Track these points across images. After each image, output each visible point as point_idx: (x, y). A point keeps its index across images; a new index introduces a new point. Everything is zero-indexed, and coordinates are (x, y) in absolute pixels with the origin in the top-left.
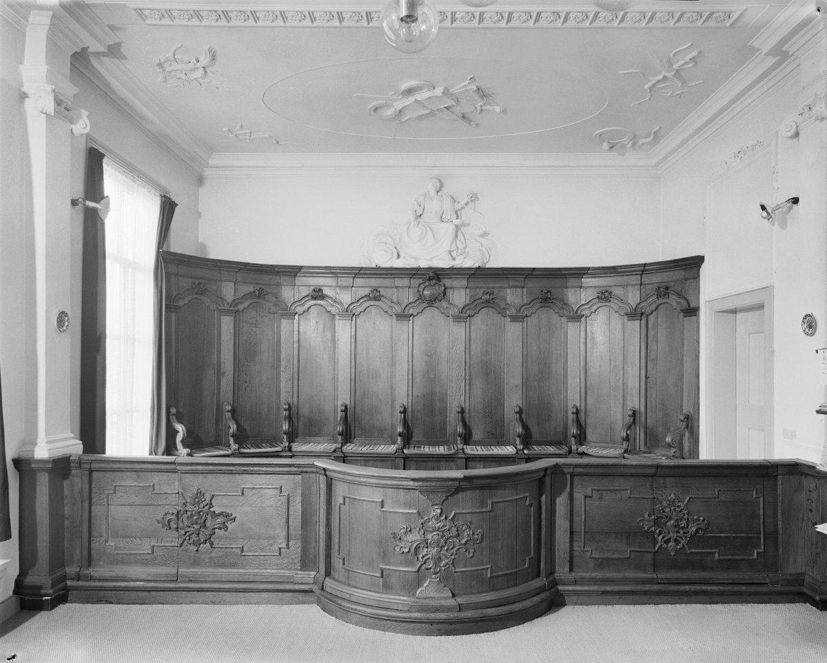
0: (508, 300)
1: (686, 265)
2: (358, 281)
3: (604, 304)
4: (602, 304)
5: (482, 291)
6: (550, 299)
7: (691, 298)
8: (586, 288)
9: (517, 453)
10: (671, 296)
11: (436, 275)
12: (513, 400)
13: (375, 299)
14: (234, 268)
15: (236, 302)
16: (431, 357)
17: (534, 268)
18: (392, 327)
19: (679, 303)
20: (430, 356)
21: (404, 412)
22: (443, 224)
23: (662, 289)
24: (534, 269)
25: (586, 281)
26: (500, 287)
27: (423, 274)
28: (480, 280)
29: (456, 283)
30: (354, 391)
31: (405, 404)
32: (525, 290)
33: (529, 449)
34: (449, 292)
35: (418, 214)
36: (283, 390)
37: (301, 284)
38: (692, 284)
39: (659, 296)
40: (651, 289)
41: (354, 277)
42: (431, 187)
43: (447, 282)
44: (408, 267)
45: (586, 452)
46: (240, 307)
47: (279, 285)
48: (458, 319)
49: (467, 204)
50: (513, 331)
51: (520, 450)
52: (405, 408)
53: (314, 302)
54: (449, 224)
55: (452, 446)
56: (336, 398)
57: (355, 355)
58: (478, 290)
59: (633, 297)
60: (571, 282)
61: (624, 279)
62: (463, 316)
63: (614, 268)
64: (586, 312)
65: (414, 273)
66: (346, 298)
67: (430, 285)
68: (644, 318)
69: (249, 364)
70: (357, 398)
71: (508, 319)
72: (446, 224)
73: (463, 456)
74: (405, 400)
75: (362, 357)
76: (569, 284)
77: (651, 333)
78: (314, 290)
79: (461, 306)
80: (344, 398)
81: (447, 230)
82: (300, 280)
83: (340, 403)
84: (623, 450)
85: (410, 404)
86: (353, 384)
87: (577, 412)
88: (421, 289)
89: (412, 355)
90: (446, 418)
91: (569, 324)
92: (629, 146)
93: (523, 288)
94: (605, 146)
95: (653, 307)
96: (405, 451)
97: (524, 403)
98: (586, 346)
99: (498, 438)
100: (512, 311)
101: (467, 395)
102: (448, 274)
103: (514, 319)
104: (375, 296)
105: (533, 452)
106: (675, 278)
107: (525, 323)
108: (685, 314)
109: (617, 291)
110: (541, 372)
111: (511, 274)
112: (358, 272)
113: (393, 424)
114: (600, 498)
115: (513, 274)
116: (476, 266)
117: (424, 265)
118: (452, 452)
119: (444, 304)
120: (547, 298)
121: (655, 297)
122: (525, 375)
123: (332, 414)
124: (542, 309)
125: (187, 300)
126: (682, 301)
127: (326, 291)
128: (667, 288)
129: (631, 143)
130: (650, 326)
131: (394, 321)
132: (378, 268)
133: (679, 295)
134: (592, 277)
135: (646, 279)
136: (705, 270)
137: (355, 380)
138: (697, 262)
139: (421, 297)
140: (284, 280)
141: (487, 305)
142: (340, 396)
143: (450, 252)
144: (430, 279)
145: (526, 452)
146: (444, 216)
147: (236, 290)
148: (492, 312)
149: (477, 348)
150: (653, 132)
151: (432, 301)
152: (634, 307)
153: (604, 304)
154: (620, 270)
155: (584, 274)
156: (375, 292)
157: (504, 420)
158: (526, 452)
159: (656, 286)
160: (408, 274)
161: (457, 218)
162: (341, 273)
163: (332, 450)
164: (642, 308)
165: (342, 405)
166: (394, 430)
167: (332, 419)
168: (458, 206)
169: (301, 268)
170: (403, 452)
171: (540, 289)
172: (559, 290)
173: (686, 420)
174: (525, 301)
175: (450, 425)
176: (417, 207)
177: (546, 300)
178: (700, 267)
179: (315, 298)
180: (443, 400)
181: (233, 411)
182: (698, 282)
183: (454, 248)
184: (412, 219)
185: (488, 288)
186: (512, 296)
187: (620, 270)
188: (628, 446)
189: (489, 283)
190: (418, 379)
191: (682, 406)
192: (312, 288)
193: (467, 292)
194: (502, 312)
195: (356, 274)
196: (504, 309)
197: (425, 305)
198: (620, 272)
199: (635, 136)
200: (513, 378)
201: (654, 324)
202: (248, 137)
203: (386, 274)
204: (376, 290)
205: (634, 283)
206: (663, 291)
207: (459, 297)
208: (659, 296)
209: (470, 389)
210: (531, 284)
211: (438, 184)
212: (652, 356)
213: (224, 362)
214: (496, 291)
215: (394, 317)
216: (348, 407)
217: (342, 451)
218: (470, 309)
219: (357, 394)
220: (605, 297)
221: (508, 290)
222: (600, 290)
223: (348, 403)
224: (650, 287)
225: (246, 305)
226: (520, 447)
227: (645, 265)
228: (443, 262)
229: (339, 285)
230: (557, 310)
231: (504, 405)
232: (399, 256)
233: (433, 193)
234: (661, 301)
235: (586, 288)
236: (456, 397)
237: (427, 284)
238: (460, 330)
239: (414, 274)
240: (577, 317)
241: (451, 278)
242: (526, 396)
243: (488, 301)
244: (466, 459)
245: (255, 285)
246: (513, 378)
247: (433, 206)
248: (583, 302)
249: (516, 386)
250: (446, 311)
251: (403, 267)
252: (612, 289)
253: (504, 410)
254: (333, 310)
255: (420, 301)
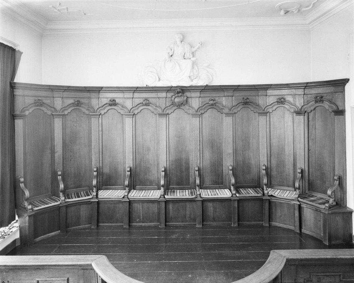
0: (224, 103)
1: (335, 84)
2: (136, 95)
3: (280, 105)
4: (279, 106)
5: (208, 99)
6: (248, 102)
7: (339, 103)
8: (270, 96)
9: (232, 196)
10: (324, 102)
11: (182, 90)
12: (228, 163)
13: (147, 105)
14: (62, 89)
15: (64, 109)
16: (180, 139)
17: (239, 85)
18: (156, 121)
19: (329, 106)
20: (179, 137)
21: (165, 171)
22: (185, 60)
23: (318, 98)
24: (239, 86)
25: (269, 92)
26: (219, 96)
27: (174, 90)
28: (208, 92)
29: (193, 94)
30: (135, 159)
31: (165, 166)
32: (234, 97)
33: (239, 193)
34: (190, 100)
35: (171, 55)
36: (93, 159)
37: (102, 97)
38: (340, 95)
39: (316, 102)
40: (311, 97)
41: (304, 88)
42: (178, 39)
43: (188, 94)
44: (165, 86)
45: (273, 195)
46: (66, 112)
47: (90, 98)
48: (194, 115)
49: (198, 48)
50: (228, 121)
51: (234, 194)
52: (165, 168)
53: (110, 107)
54: (188, 60)
55: (193, 190)
56: (125, 163)
57: (135, 137)
58: (206, 99)
59: (299, 102)
60: (261, 93)
61: (294, 91)
62: (199, 113)
63: (287, 84)
64: (271, 110)
65: (169, 89)
66: (129, 104)
67: (178, 96)
68: (306, 114)
69: (72, 145)
70: (137, 163)
71: (224, 115)
72: (187, 60)
73: (200, 199)
74: (165, 163)
75: (140, 139)
76: (259, 94)
77: (311, 123)
78: (110, 100)
79: (196, 108)
80: (129, 163)
81: (187, 64)
82: (102, 95)
83: (127, 166)
84: (297, 196)
85: (168, 168)
86: (134, 155)
87: (266, 169)
88: (173, 99)
89: (169, 137)
90: (189, 173)
91: (260, 117)
92: (295, 12)
93: (232, 96)
94: (282, 12)
95: (312, 108)
96: (166, 197)
97: (234, 163)
98: (270, 130)
99: (219, 183)
100: (226, 111)
101: (201, 160)
102: (189, 90)
103: (228, 115)
104: (147, 103)
105: (242, 195)
106: (327, 91)
107: (234, 117)
108: (336, 114)
109: (289, 98)
110: (243, 144)
111: (225, 89)
112: (136, 90)
113: (158, 178)
114: (318, 281)
115: (227, 89)
116: (205, 84)
117: (174, 84)
118: (194, 196)
119: (187, 107)
120: (247, 102)
121: (314, 102)
122: (234, 148)
123: (123, 172)
124: (244, 109)
125: (31, 111)
126: (333, 105)
127: (118, 101)
128: (322, 97)
129: (297, 11)
130: (310, 120)
131: (158, 117)
132: (147, 87)
133: (330, 102)
134: (273, 90)
135: (307, 91)
136: (348, 87)
137: (135, 152)
138: (345, 82)
139: (173, 104)
140: (93, 95)
141: (212, 107)
142: (127, 162)
143: (190, 77)
144: (178, 93)
145: (237, 195)
146: (185, 56)
147: (63, 102)
148: (214, 111)
149: (206, 132)
150: (313, 3)
151: (180, 105)
152: (300, 108)
153: (280, 105)
154: (291, 86)
155: (268, 88)
156: (146, 101)
157: (223, 174)
158: (237, 195)
159: (314, 96)
160: (132, 90)
161: (193, 56)
162: (126, 90)
163: (122, 196)
164: (305, 109)
165: (128, 167)
166: (159, 182)
167: (123, 174)
168: (193, 50)
169: (102, 88)
170: (164, 197)
171: (243, 97)
172: (254, 97)
173: (338, 180)
174: (234, 105)
175: (192, 177)
176: (169, 51)
177: (246, 103)
178: (346, 85)
179: (110, 105)
180: (187, 163)
181: (63, 175)
182: (344, 95)
183: (192, 74)
184: (167, 58)
185: (212, 97)
186: (225, 101)
187: (291, 86)
188: (299, 192)
189: (212, 94)
190: (172, 151)
191: (334, 170)
192: (109, 99)
193: (200, 100)
194: (220, 111)
195: (135, 91)
196: (222, 109)
197: (176, 108)
198: (291, 87)
199: (301, 6)
200: (228, 149)
201: (313, 118)
202: (66, 11)
203: (152, 90)
204: (146, 99)
205: (300, 93)
206: (319, 99)
207: (195, 102)
208: (316, 102)
209: (202, 156)
210: (237, 94)
211: (182, 37)
212: (312, 137)
213: (56, 146)
214: (217, 99)
215: (158, 115)
216: (132, 169)
217: (128, 198)
218: (201, 110)
219: (137, 160)
220: (281, 102)
221: (224, 98)
222: (278, 97)
223: (132, 166)
224: (309, 96)
225: (69, 110)
226: (234, 192)
227: (307, 83)
228: (186, 83)
229: (125, 97)
230: (252, 109)
231: (222, 165)
232: (159, 79)
233: (179, 43)
234: (317, 105)
235: (270, 96)
236: (195, 162)
237: (176, 95)
238: (196, 121)
239: (169, 90)
240: (265, 113)
241: (190, 92)
242: (235, 160)
243: (212, 105)
244: (202, 201)
245: (75, 99)
246: (228, 149)
247: (179, 50)
248: (268, 104)
249: (230, 154)
250: (188, 111)
251: (162, 86)
252: (285, 97)
253: (223, 168)
254: (122, 112)
255: (173, 105)
